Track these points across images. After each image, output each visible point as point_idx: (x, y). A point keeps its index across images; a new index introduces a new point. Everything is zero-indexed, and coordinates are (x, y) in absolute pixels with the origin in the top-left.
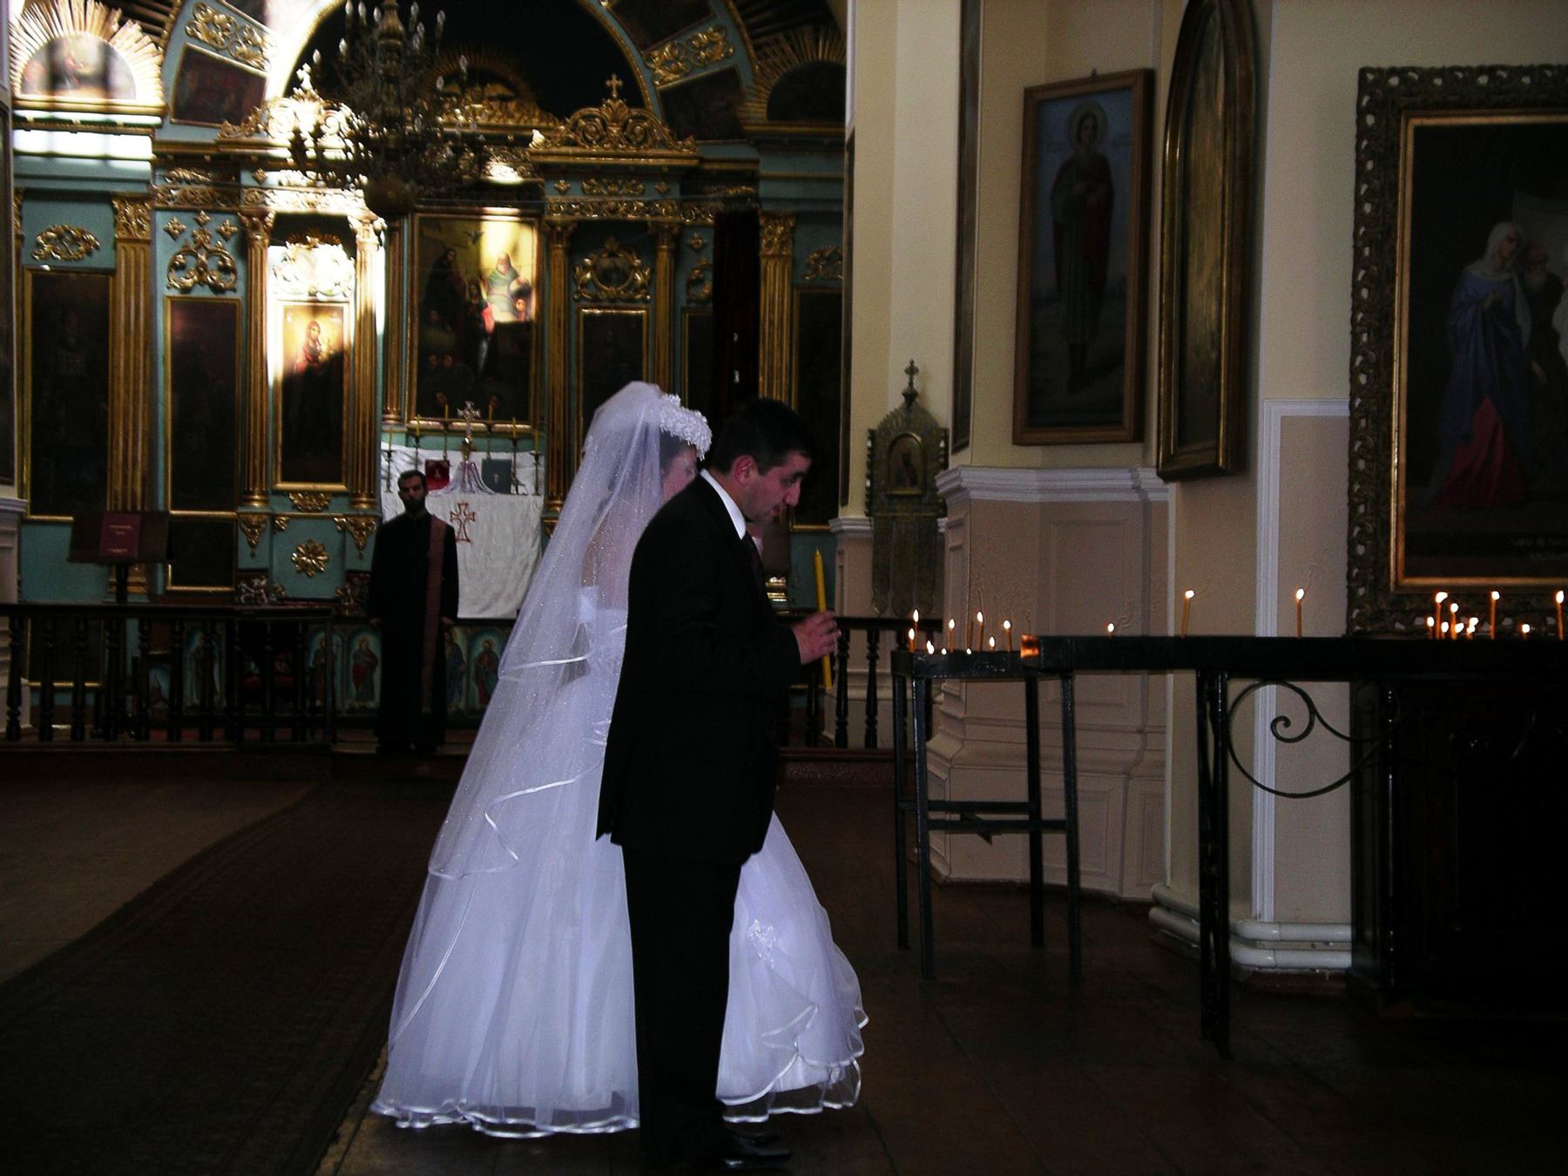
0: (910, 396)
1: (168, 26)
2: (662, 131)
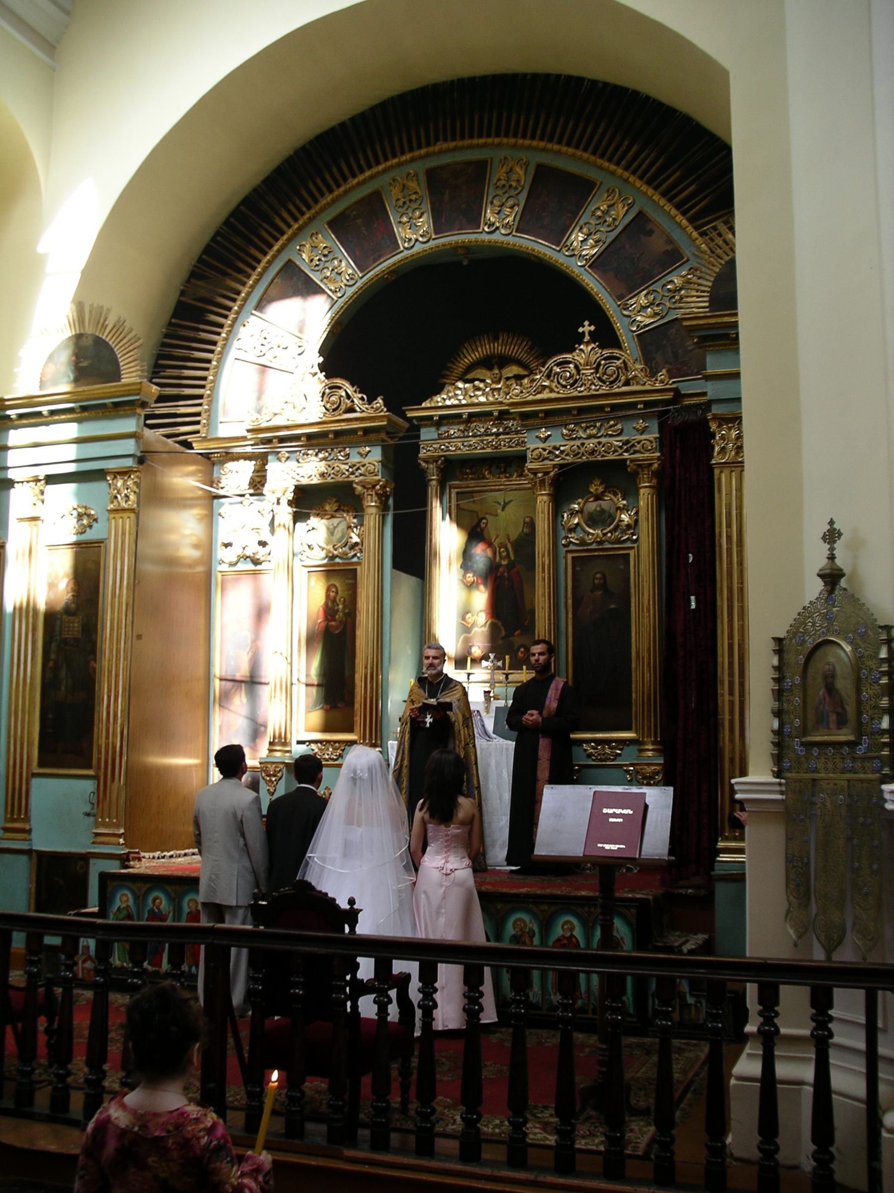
0: (832, 577)
1: (220, 344)
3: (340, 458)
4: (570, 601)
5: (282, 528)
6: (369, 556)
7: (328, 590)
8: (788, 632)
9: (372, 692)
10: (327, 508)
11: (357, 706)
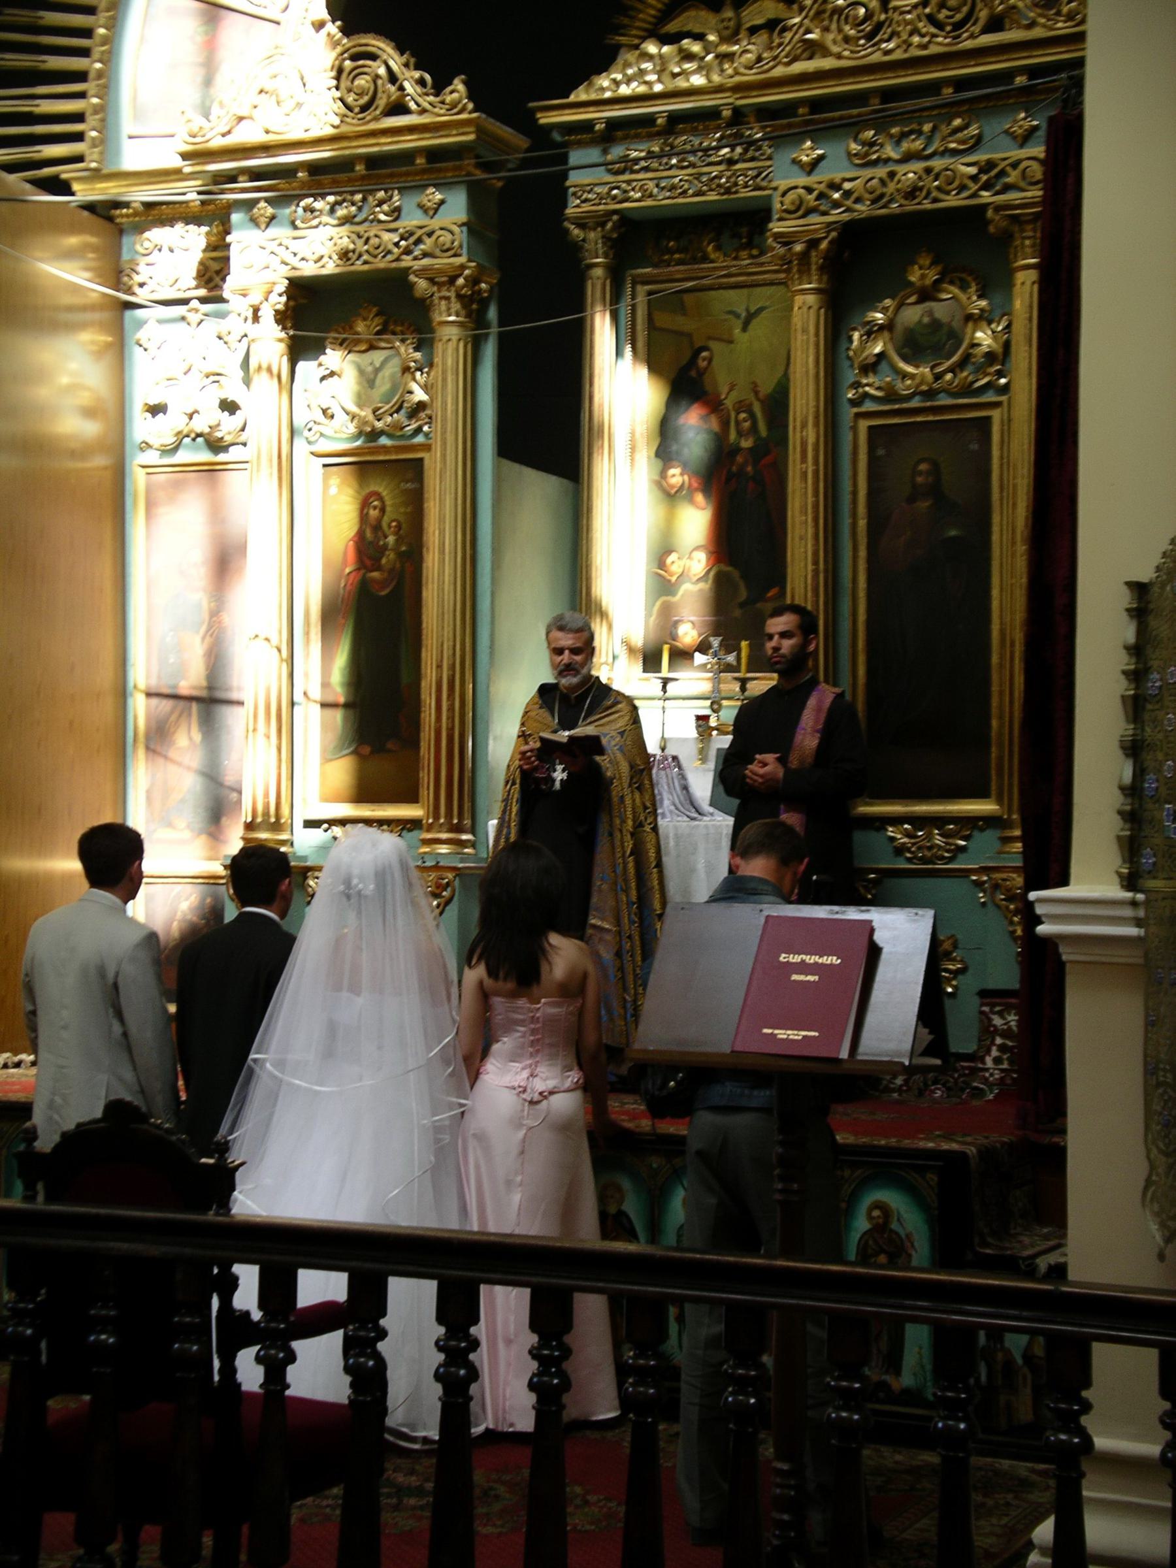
3: (382, 217)
4: (862, 523)
5: (264, 374)
6: (444, 433)
7: (364, 505)
8: (1158, 569)
9: (451, 718)
10: (360, 327)
11: (423, 745)
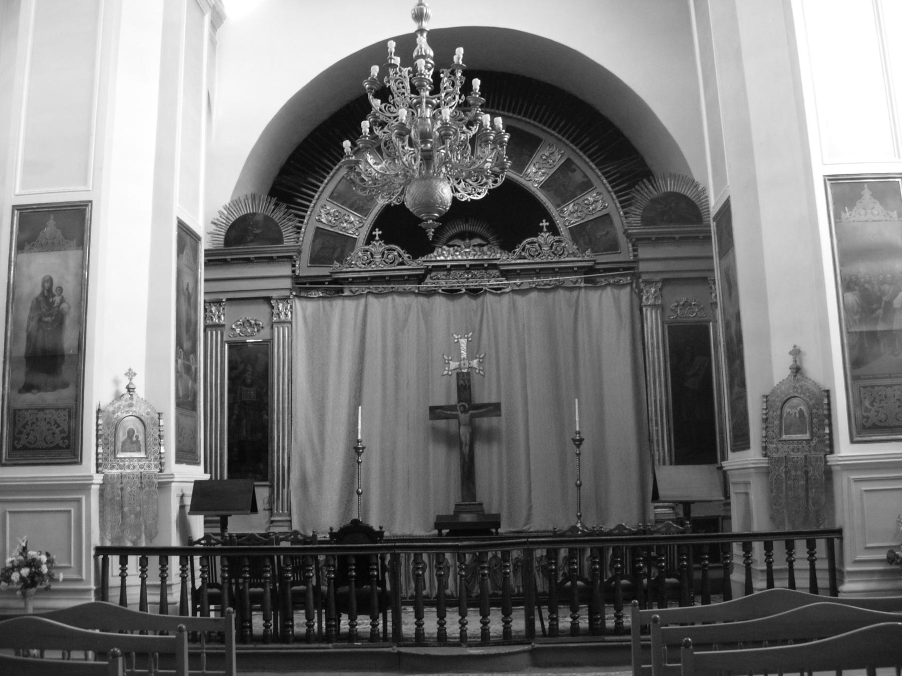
0: (797, 370)
2: (572, 247)
